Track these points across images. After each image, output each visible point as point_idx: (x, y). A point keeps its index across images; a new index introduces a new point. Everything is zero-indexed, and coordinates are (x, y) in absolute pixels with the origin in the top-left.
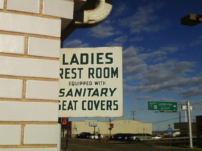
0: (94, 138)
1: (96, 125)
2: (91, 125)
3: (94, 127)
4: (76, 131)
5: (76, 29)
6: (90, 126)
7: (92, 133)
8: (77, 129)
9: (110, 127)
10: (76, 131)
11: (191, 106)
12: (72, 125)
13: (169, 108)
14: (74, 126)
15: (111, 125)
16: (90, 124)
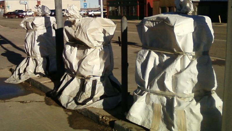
0: (26, 14)
1: (27, 3)
2: (22, 3)
3: (25, 5)
4: (9, 9)
5: (103, 94)
6: (21, 4)
7: (24, 10)
8: (9, 7)
9: (37, 4)
10: (9, 9)
11: (199, 4)
12: (5, 4)
13: (157, 23)
14: (7, 4)
15: (38, 3)
16: (21, 2)
